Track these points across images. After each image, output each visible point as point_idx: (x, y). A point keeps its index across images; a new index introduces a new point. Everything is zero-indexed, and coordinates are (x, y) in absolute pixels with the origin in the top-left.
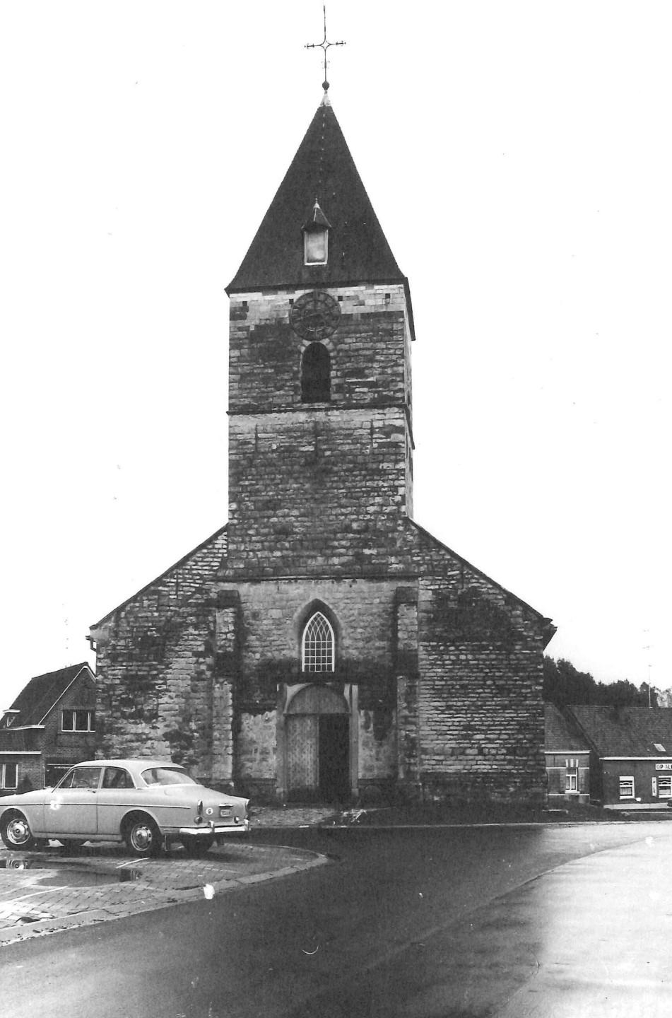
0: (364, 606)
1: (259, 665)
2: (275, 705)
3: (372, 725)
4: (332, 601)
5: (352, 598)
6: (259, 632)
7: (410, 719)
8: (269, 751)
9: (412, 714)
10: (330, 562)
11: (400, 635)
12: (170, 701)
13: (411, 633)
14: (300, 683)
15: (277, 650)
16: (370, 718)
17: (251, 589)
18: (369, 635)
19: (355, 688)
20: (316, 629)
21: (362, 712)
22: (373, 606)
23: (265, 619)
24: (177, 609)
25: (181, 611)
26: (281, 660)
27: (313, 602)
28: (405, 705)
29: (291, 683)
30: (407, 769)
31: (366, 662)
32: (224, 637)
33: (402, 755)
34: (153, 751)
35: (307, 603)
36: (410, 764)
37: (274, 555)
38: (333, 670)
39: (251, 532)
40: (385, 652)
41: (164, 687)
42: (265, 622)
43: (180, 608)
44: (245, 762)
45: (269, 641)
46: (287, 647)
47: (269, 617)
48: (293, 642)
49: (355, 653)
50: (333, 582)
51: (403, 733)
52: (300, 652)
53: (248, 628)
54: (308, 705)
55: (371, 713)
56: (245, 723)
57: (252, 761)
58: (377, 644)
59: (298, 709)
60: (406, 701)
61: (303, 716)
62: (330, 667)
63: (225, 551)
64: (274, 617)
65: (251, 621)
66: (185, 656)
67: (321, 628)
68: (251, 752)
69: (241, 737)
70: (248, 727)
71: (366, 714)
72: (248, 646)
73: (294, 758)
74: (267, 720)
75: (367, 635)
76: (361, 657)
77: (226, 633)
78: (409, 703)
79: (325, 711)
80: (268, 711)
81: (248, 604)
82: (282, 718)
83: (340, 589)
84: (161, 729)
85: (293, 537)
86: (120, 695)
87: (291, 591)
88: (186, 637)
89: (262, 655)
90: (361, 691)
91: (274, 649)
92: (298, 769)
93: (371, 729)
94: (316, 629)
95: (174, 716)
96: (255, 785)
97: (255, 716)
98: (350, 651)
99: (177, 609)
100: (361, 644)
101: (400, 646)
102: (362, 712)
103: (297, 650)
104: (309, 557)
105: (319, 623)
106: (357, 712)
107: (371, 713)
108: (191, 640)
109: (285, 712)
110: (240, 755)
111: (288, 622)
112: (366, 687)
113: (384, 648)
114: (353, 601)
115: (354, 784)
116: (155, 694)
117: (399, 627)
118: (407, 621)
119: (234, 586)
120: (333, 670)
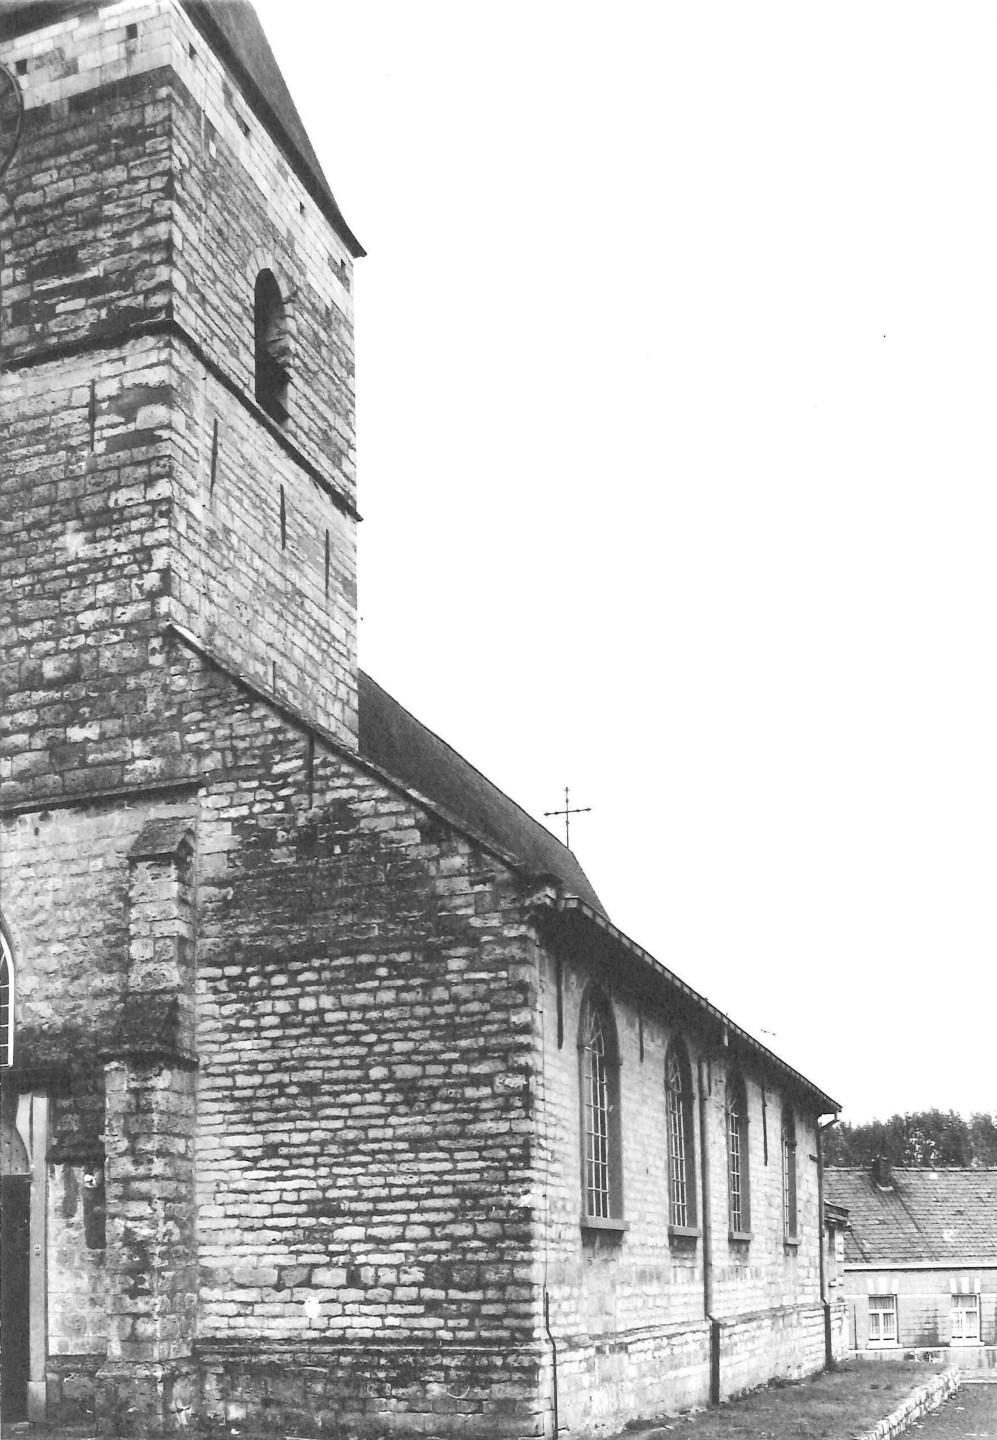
3: (80, 1207)
9: (142, 1170)
13: (161, 943)
19: (41, 1104)
22: (89, 879)
28: (124, 1145)
30: (128, 1330)
31: (70, 1033)
33: (119, 1288)
36: (136, 1316)
49: (44, 1009)
51: (118, 1226)
60: (126, 1133)
76: (59, 1021)
78: (133, 1138)
100: (58, 985)
102: (59, 1169)
112: (65, 1103)
115: (37, 1365)
118: (151, 910)
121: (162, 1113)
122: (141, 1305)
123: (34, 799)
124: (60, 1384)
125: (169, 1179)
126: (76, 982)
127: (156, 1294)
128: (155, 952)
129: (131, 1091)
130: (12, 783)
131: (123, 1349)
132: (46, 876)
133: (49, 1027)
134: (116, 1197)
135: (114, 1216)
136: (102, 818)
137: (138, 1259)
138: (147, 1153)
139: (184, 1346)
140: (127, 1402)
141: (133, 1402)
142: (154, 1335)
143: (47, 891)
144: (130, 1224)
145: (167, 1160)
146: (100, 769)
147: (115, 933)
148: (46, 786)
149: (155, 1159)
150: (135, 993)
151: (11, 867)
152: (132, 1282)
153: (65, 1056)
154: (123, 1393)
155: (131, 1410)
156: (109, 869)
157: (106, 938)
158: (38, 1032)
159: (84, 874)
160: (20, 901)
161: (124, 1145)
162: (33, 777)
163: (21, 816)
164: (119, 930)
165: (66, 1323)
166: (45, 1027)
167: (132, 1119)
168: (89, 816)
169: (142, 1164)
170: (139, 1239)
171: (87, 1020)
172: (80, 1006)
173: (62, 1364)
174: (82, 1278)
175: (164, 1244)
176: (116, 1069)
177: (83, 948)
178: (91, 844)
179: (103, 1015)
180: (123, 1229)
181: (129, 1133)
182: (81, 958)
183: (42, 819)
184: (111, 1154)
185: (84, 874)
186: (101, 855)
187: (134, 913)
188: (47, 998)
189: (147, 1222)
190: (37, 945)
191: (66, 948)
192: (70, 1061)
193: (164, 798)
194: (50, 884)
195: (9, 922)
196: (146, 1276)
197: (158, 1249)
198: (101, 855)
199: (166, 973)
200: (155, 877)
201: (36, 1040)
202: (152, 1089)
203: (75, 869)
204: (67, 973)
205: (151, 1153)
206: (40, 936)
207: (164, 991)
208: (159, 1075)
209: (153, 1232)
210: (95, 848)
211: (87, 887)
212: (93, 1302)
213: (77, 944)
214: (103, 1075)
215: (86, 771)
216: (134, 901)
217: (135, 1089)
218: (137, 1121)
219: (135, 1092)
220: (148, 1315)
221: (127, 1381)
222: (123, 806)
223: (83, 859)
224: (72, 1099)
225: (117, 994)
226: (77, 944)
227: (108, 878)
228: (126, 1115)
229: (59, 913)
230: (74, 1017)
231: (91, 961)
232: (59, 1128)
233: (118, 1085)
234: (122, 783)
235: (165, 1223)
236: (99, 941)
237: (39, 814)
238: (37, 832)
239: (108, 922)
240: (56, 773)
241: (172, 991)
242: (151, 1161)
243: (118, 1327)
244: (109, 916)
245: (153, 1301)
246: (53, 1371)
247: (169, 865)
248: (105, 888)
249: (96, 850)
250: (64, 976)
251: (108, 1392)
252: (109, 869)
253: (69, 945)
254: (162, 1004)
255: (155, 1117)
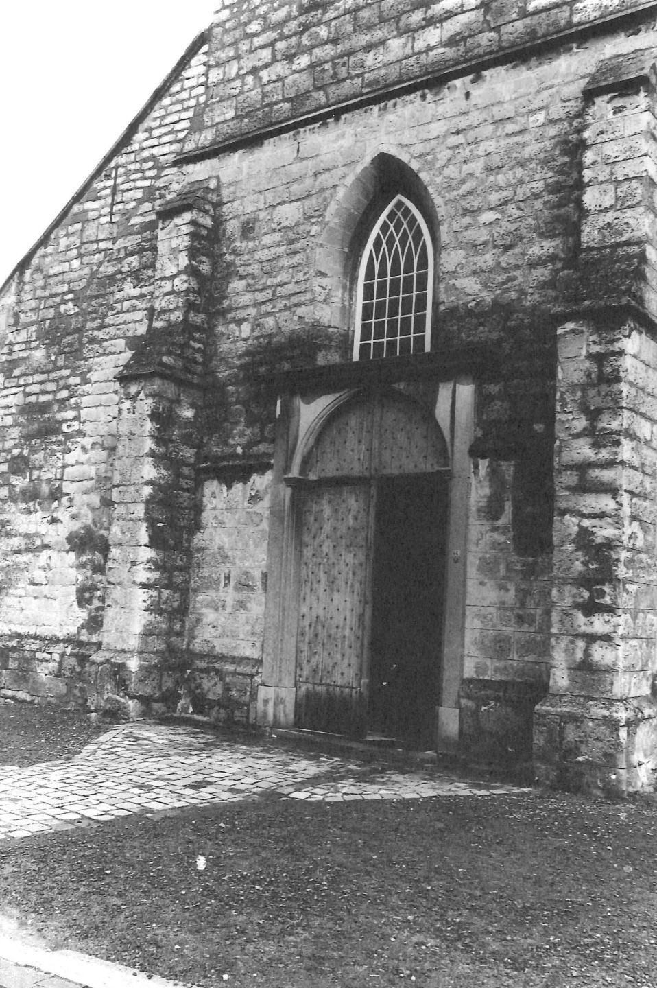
0: (502, 143)
1: (247, 353)
2: (270, 456)
3: (508, 506)
4: (419, 149)
5: (471, 128)
6: (254, 269)
7: (596, 473)
8: (253, 579)
9: (604, 454)
10: (420, 45)
11: (590, 198)
12: (84, 458)
13: (625, 186)
14: (334, 392)
15: (287, 308)
16: (503, 483)
17: (245, 164)
18: (512, 227)
19: (466, 391)
20: (390, 242)
21: (484, 464)
22: (527, 137)
23: (265, 234)
24: (109, 245)
25: (116, 247)
26: (293, 332)
27: (373, 160)
28: (581, 423)
29: (310, 394)
30: (579, 655)
31: (502, 309)
32: (168, 286)
33: (568, 601)
34: (49, 574)
35: (359, 168)
36: (591, 638)
37: (295, 67)
38: (428, 348)
39: (254, 27)
40: (557, 271)
41: (76, 425)
42: (266, 240)
43: (114, 240)
44: (204, 610)
45: (270, 287)
46: (308, 296)
47: (274, 226)
48: (325, 281)
49: (471, 285)
50: (423, 97)
51: (572, 524)
52: (347, 312)
53: (232, 263)
54: (351, 455)
55: (508, 469)
56: (209, 507)
57: (218, 607)
58: (535, 250)
59: (329, 468)
60: (585, 409)
61: (339, 483)
62: (420, 341)
63: (202, 90)
64: (285, 223)
65: (238, 244)
66: (113, 349)
67: (403, 240)
68: (217, 582)
69: (202, 544)
70: (216, 517)
71: (494, 473)
72: (231, 309)
73: (315, 605)
74: (252, 497)
75: (507, 226)
76: (488, 297)
77: (172, 278)
78: (593, 415)
79: (393, 470)
80: (256, 471)
81: (236, 204)
82: (287, 493)
83: (440, 109)
84: (68, 526)
85: (337, 9)
86: (9, 451)
87: (324, 149)
88: (118, 306)
89: (257, 325)
90: (482, 402)
91: (280, 305)
92: (322, 634)
93: (505, 519)
94: (390, 242)
95: (86, 492)
96: (217, 672)
97: (229, 487)
98: (459, 283)
99: (109, 245)
100: (487, 259)
101: (590, 234)
102: (484, 464)
103: (333, 303)
104: (368, 48)
105: (398, 227)
106: (468, 463)
107: (508, 469)
108: (128, 311)
109: (295, 472)
110: (195, 591)
111: (314, 229)
112: (494, 389)
113: (553, 258)
114: (471, 135)
115: (450, 689)
116: (60, 443)
117: (588, 174)
118: (612, 150)
119: (213, 168)
120: (428, 348)
121: (631, 384)
122: (599, 625)
123: (466, 61)
124: (476, 712)
125: (635, 468)
126: (510, 252)
127: (620, 612)
128: (617, 198)
129: (590, 356)
130: (442, 50)
131: (572, 680)
132: (477, 142)
133: (478, 304)
134: (568, 488)
135: (563, 513)
136: (545, 68)
137: (595, 566)
138: (612, 433)
139: (644, 682)
140: (577, 748)
141: (583, 748)
142: (615, 664)
143: (479, 157)
144: (586, 523)
145: (634, 444)
146: (544, 15)
147: (559, 191)
148: (479, 45)
149: (623, 441)
150: (590, 249)
151: (438, 137)
152: (586, 595)
153: (495, 336)
154: (571, 734)
155: (580, 759)
156: (552, 122)
157: (546, 199)
158: (462, 312)
159: (521, 132)
160: (447, 172)
161: (581, 423)
162: (464, 39)
163: (450, 83)
164: (564, 188)
165: (486, 642)
166: (472, 304)
167: (592, 392)
168: (529, 69)
169: (605, 446)
170: (598, 541)
171: (522, 292)
172: (514, 279)
173: (476, 687)
174: (508, 590)
175: (629, 550)
176: (573, 331)
177: (519, 213)
178: (530, 97)
179: (543, 286)
180: (576, 529)
181: (588, 408)
182: (516, 225)
183: (473, 81)
184: (562, 435)
185: (521, 132)
186: (541, 109)
187: (589, 157)
188: (474, 273)
189: (610, 520)
190: (464, 215)
191: (499, 216)
192: (500, 341)
193: (624, 30)
194: (481, 150)
195: (433, 196)
196: (607, 588)
197: (624, 555)
198: (541, 109)
199: (631, 221)
200: (618, 110)
201: (461, 319)
202: (621, 353)
203: (510, 128)
204: (499, 243)
205: (618, 433)
206: (468, 206)
207: (628, 243)
208: (629, 336)
209: (616, 532)
210: (535, 102)
211: (524, 145)
212: (521, 620)
213: (512, 210)
214: (555, 339)
215: (527, 21)
216: (590, 142)
217: (598, 354)
218: (599, 393)
219: (598, 358)
220: (607, 638)
221: (577, 720)
222: (571, 49)
223: (521, 115)
224: (502, 383)
225: (560, 260)
226: (512, 210)
227: (552, 131)
228: (584, 388)
229: (492, 178)
230: (507, 290)
231: (528, 227)
232: (484, 417)
233: (575, 352)
234: (570, 24)
235: (630, 524)
236: (538, 204)
237: (471, 77)
238: (468, 95)
239: (550, 181)
240: (491, 30)
241: (639, 243)
242: (617, 443)
243: (566, 651)
244: (551, 174)
245: (615, 620)
246: (468, 697)
247: (637, 93)
248: (547, 143)
249: (537, 104)
250: (495, 247)
251: (550, 732)
252: (552, 122)
253: (503, 212)
254: (629, 257)
255: (624, 388)
